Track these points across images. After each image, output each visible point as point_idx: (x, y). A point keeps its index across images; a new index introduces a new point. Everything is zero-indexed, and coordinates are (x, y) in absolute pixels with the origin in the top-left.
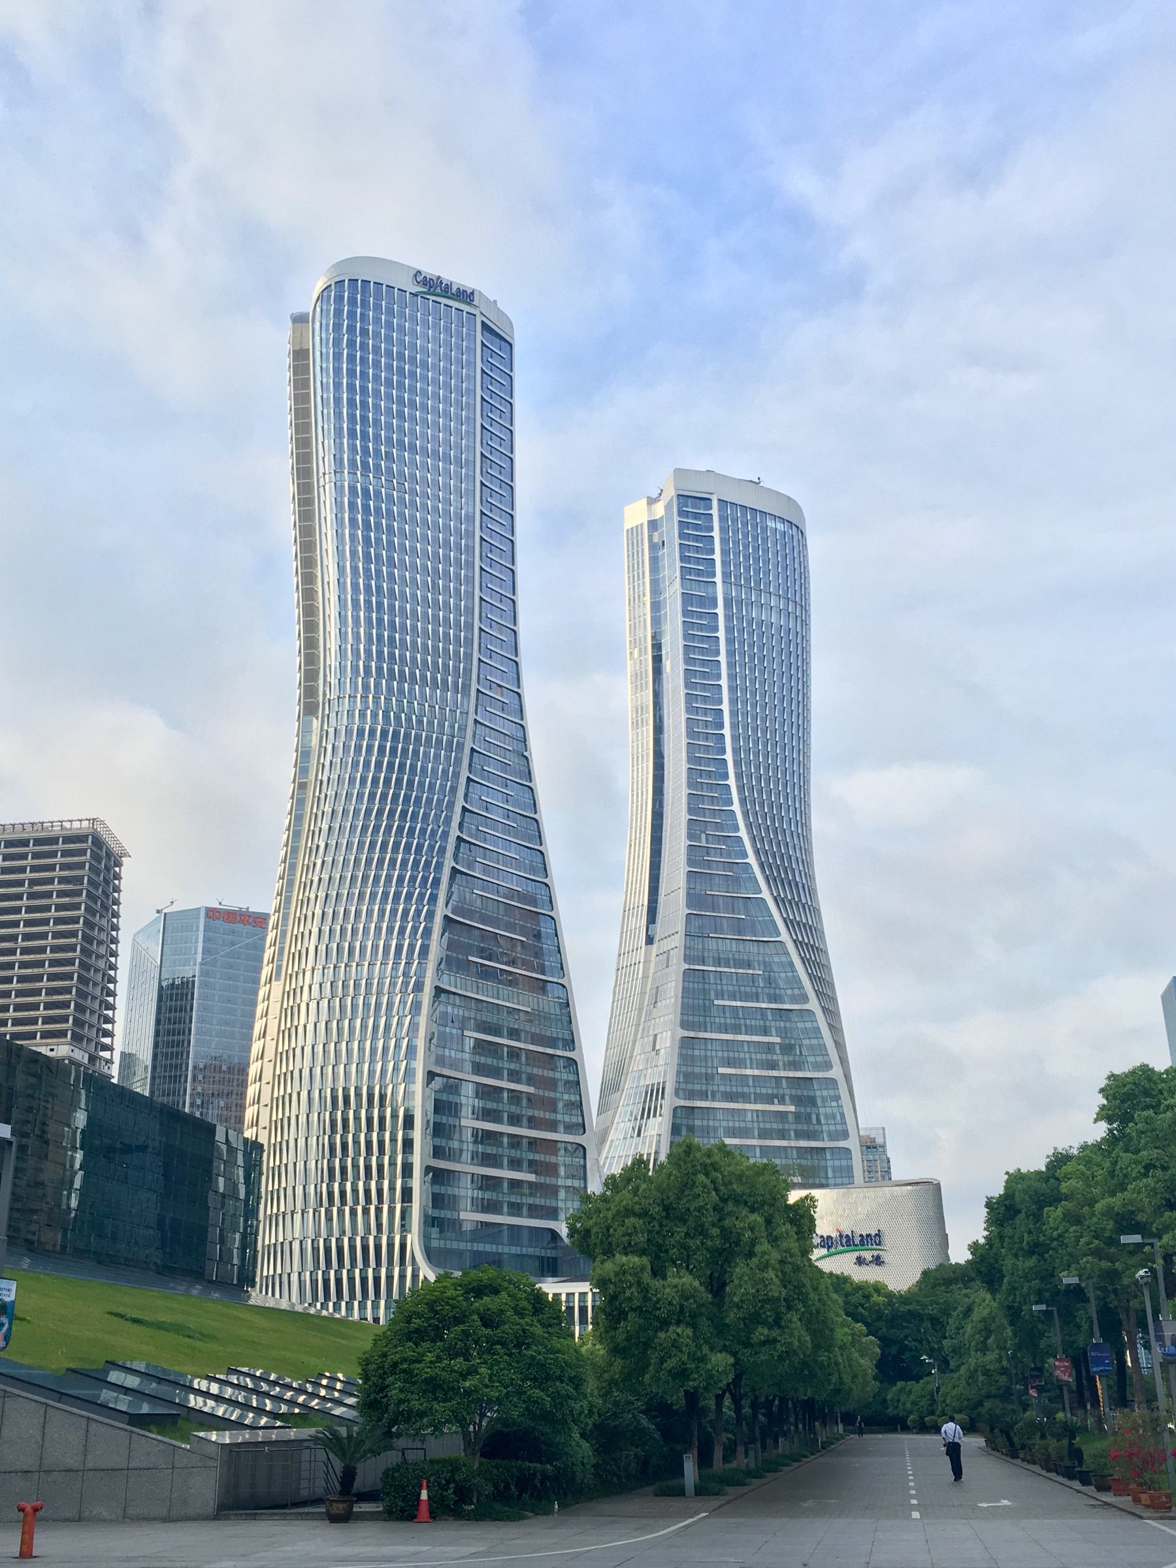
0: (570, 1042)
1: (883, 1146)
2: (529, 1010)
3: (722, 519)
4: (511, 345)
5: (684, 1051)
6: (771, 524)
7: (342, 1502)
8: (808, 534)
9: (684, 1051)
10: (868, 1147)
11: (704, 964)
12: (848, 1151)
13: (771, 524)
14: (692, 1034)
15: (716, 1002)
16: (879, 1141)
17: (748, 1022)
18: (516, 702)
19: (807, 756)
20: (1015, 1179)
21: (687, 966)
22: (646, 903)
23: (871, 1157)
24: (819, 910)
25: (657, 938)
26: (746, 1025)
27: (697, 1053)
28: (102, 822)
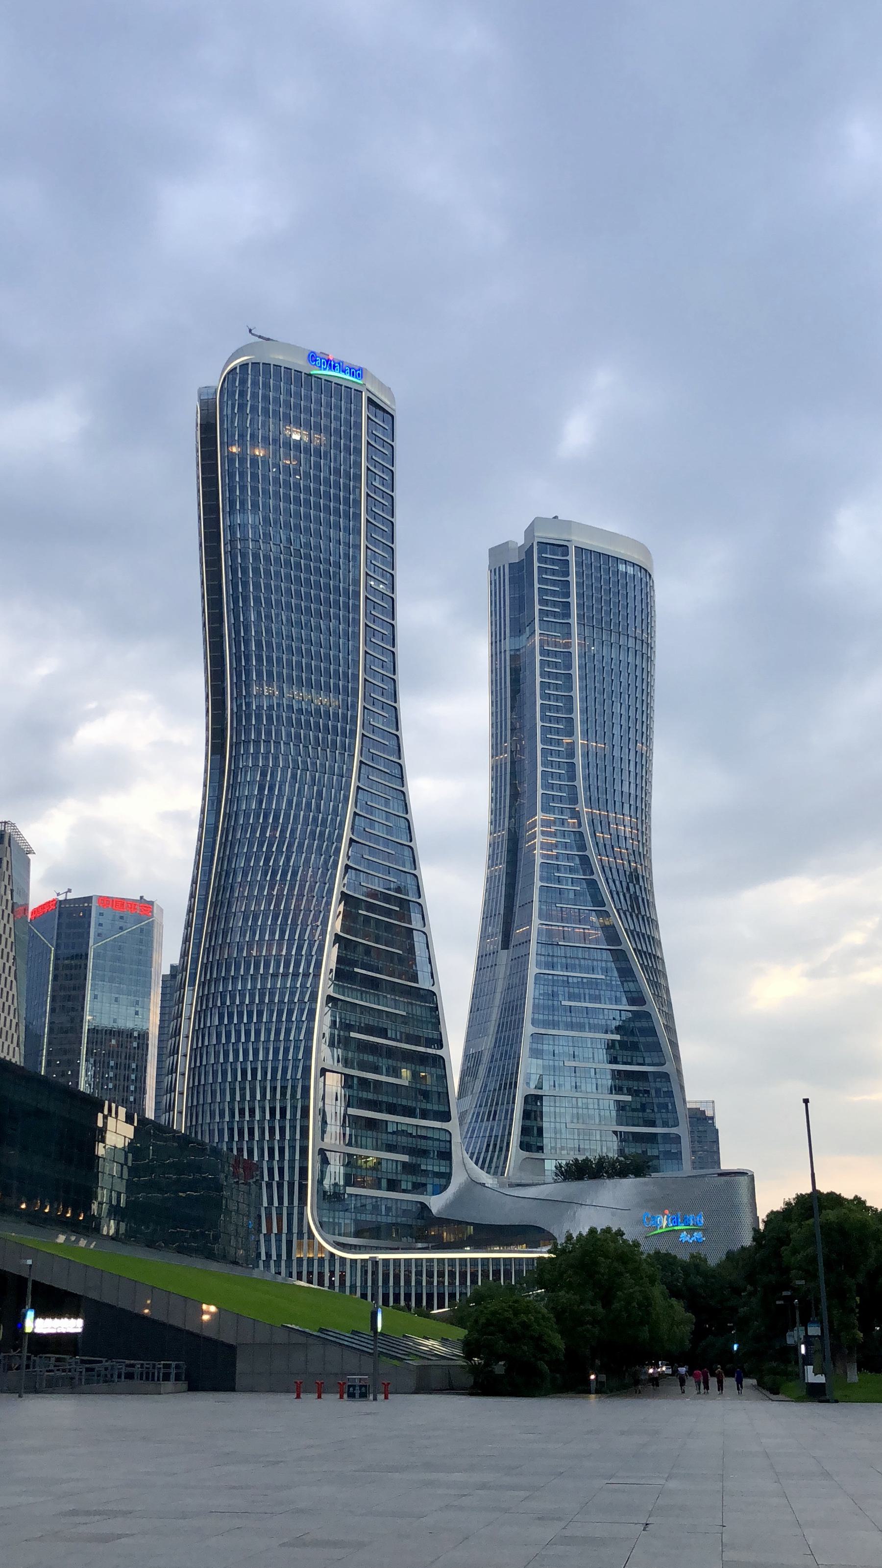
0: (439, 1043)
1: (712, 1118)
2: (404, 1014)
3: (579, 564)
4: (393, 417)
5: (535, 1046)
6: (622, 567)
7: (450, 1387)
8: (655, 576)
9: (535, 1046)
10: (698, 1119)
11: (553, 968)
12: (677, 1139)
13: (622, 567)
14: (543, 1031)
15: (563, 1003)
16: (709, 1113)
17: (591, 1021)
18: (395, 742)
19: (648, 828)
20: (772, 1212)
21: (538, 971)
22: (502, 912)
23: (701, 1128)
24: (657, 921)
25: (512, 944)
26: (580, 965)
27: (545, 1047)
28: (13, 825)
